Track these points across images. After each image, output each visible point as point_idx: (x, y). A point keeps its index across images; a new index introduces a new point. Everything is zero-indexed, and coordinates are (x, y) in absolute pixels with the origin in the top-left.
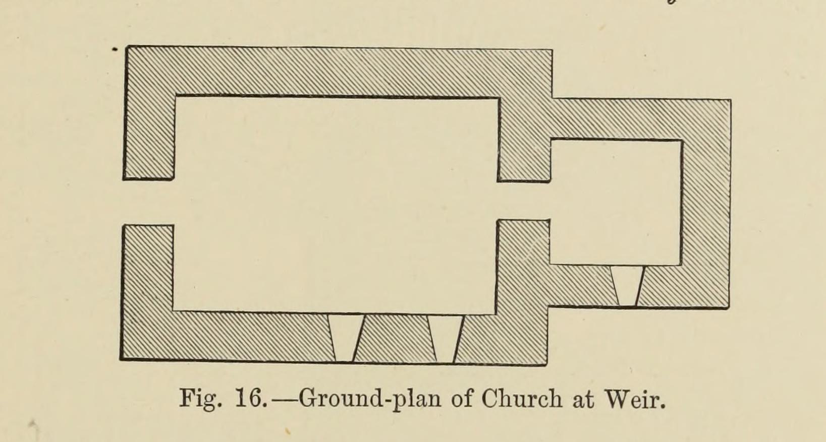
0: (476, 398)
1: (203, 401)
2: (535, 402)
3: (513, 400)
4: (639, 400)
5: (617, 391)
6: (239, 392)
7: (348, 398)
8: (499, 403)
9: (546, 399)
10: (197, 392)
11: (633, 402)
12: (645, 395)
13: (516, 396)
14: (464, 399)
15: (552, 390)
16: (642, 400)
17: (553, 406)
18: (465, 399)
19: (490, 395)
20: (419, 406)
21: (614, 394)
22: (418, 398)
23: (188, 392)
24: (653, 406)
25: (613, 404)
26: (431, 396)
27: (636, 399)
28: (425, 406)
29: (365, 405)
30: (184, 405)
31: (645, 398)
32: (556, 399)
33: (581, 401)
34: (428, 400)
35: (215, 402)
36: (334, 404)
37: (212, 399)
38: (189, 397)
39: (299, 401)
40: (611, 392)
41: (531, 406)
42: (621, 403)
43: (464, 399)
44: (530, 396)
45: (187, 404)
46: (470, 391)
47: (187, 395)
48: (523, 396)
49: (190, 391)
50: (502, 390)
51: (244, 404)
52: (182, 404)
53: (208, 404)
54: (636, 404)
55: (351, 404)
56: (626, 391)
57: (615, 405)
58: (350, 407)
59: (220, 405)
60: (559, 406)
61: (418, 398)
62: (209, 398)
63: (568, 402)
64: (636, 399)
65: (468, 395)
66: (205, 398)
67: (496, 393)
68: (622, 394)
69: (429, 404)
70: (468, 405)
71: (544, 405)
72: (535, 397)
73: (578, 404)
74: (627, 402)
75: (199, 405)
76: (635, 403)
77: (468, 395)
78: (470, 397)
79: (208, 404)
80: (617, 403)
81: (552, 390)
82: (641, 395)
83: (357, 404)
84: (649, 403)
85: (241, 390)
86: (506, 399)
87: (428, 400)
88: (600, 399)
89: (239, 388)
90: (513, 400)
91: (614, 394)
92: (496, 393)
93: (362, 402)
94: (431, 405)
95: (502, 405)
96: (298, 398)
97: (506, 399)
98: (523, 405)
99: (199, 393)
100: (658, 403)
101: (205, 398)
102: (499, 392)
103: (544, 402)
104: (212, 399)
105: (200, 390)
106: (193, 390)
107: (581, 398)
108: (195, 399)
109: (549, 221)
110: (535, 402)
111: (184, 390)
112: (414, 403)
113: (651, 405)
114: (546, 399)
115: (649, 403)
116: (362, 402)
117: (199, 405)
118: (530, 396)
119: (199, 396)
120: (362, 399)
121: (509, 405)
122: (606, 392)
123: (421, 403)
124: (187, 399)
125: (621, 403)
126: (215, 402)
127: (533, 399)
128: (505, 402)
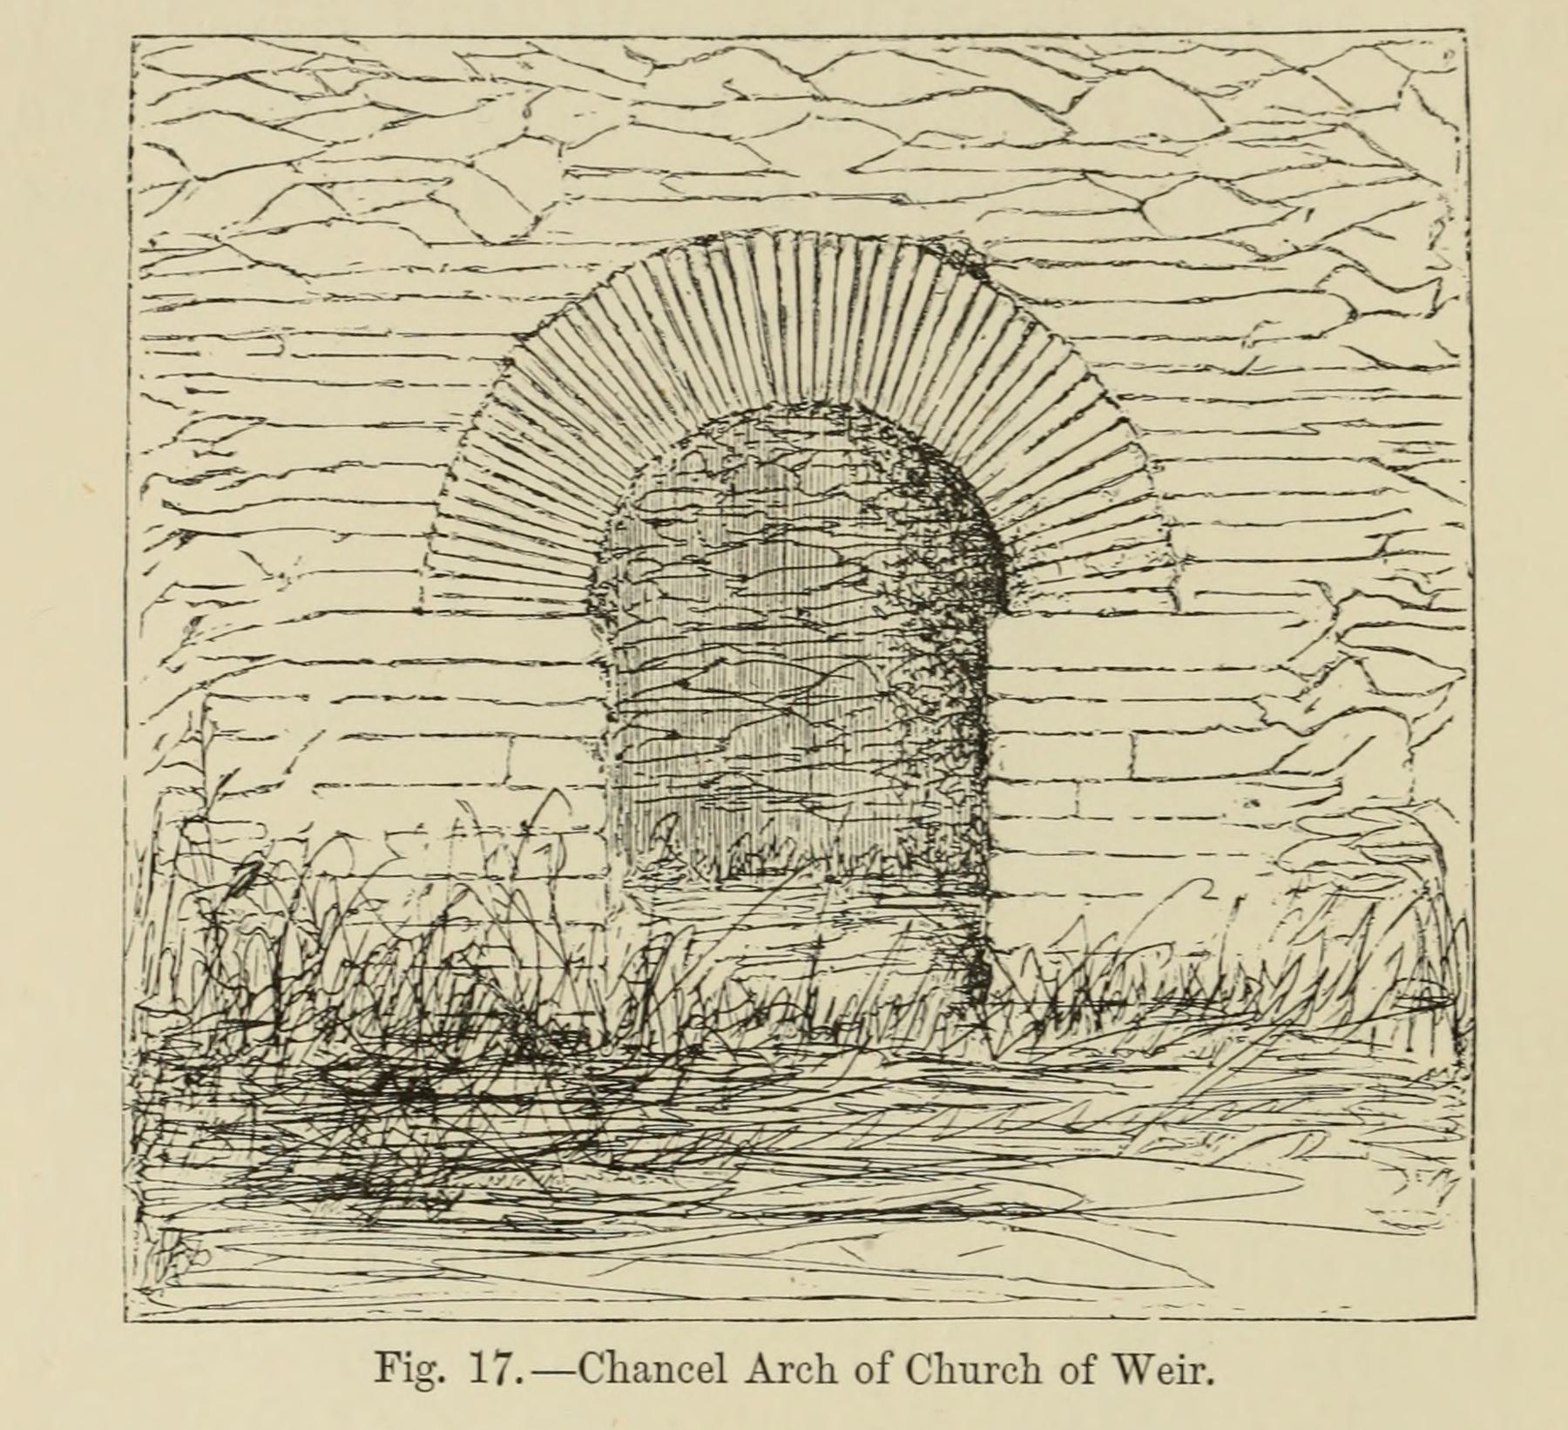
0: (896, 1369)
1: (414, 1373)
2: (997, 1374)
3: (958, 1370)
4: (1171, 1372)
5: (1134, 1356)
6: (476, 1359)
7: (970, 1370)
8: (935, 1378)
9: (1015, 1369)
10: (405, 1359)
11: (1160, 1373)
12: (1182, 1361)
13: (964, 1365)
14: (874, 1373)
15: (1025, 1355)
16: (1177, 1370)
17: (821, 1381)
18: (1082, 1370)
19: (592, 1362)
20: (637, 1381)
21: (1128, 1361)
22: (636, 1368)
23: (389, 1358)
24: (1195, 1382)
25: (1126, 1377)
26: (659, 1365)
27: (1166, 1369)
28: (648, 1381)
29: (670, 1381)
30: (383, 1379)
31: (1182, 1366)
32: (827, 1370)
33: (645, 1370)
34: (652, 1371)
35: (434, 1376)
36: (865, 1379)
37: (430, 1370)
38: (391, 1366)
39: (579, 1373)
40: (1139, 1358)
41: (990, 1381)
42: (1141, 1377)
43: (874, 1373)
44: (988, 1365)
45: (388, 1377)
46: (887, 1355)
47: (388, 1362)
48: (975, 1366)
49: (394, 1356)
50: (612, 1352)
51: (483, 1378)
52: (379, 1377)
53: (425, 1377)
54: (1166, 1378)
55: (976, 1381)
56: (1149, 1355)
57: (1146, 1379)
58: (972, 1385)
59: (442, 1379)
60: (832, 1381)
61: (636, 1368)
62: (425, 1368)
63: (1050, 1374)
64: (1166, 1369)
65: (1087, 1365)
66: (419, 1369)
67: (929, 1359)
68: (1142, 1360)
69: (655, 1378)
70: (883, 1381)
71: (805, 1379)
72: (997, 1365)
73: (640, 1377)
74: (1151, 1374)
75: (409, 1380)
76: (1164, 1376)
77: (1087, 1365)
78: (887, 1367)
79: (425, 1377)
80: (1134, 1376)
81: (820, 1355)
82: (1176, 1360)
83: (780, 1378)
84: (1189, 1377)
85: (479, 1355)
86: (946, 1371)
87: (652, 1371)
88: (1106, 1370)
89: (476, 1351)
90: (958, 1370)
91: (1128, 1361)
92: (929, 1359)
93: (665, 1377)
94: (659, 1380)
95: (940, 1381)
96: (576, 1368)
97: (946, 1371)
98: (976, 1381)
99: (408, 1360)
100: (1201, 1375)
101: (419, 1369)
102: (935, 1359)
103: (805, 1375)
104: (430, 1370)
105: (409, 1354)
106: (398, 1354)
107: (645, 1366)
108: (400, 1368)
109: (387, 834)
110: (997, 1374)
111: (383, 1354)
112: (630, 1377)
113: (986, 1379)
114: (1015, 1369)
115: (1189, 1377)
116: (665, 1376)
117: (409, 1380)
118: (988, 1365)
119: (408, 1364)
120: (665, 1370)
121: (952, 1381)
122: (1115, 1358)
123: (640, 1377)
124: (388, 1369)
125: (1141, 1377)
126: (434, 1376)
127: (788, 1369)
128: (946, 1377)
